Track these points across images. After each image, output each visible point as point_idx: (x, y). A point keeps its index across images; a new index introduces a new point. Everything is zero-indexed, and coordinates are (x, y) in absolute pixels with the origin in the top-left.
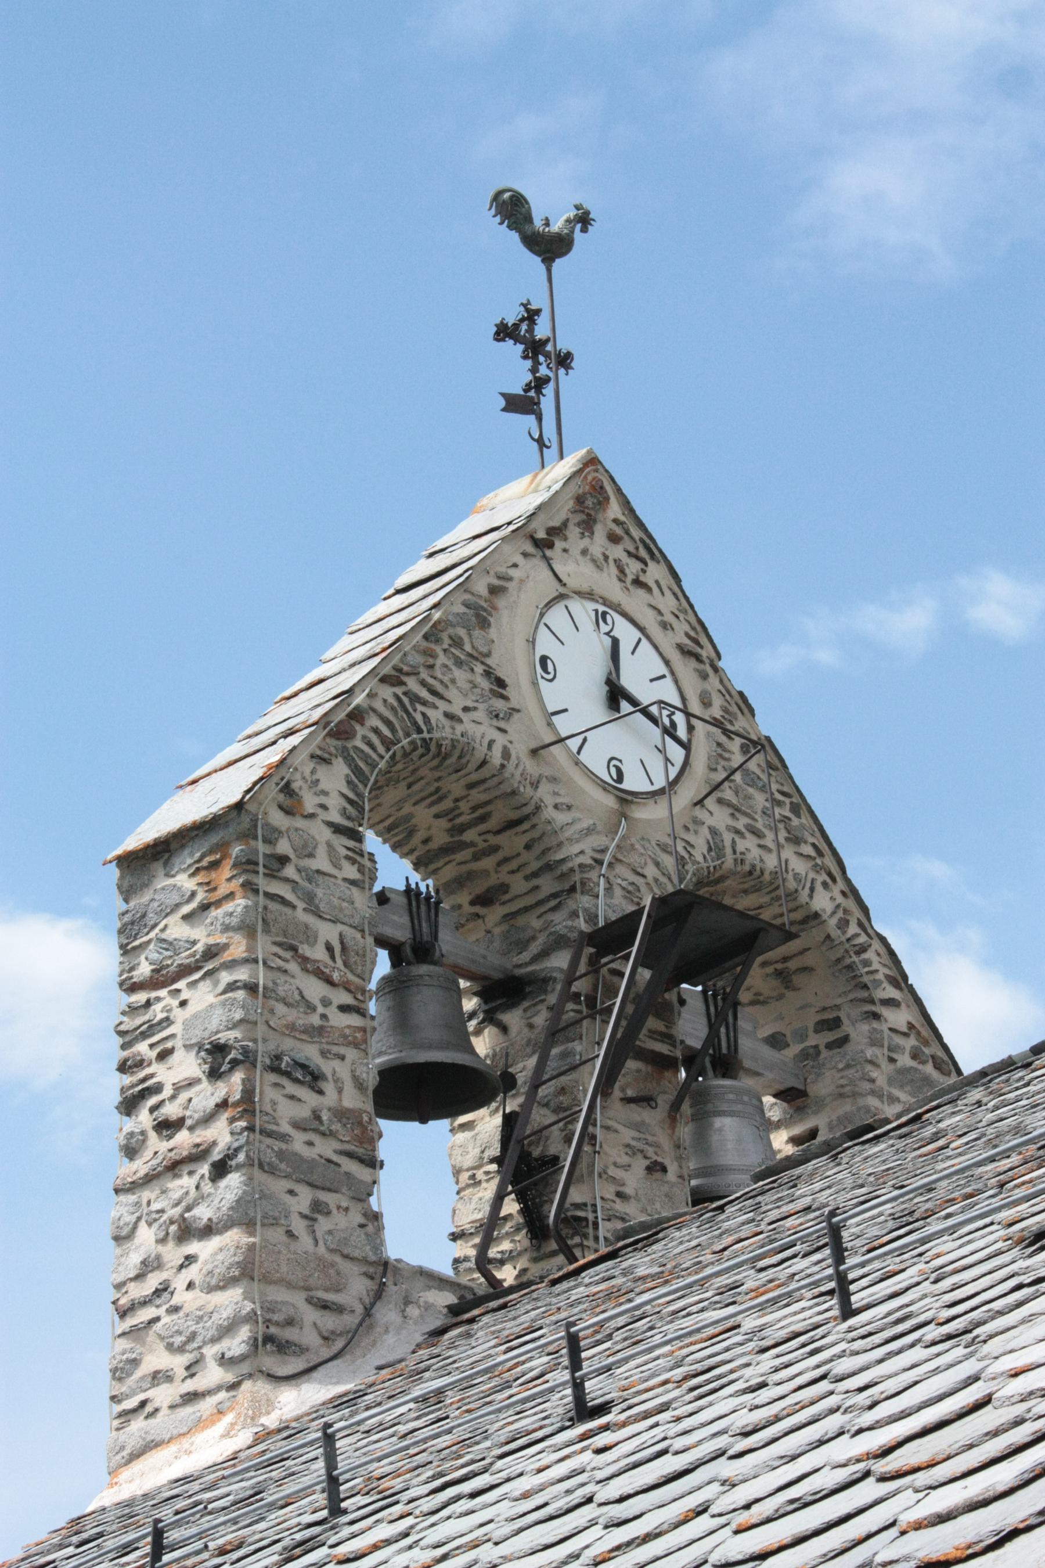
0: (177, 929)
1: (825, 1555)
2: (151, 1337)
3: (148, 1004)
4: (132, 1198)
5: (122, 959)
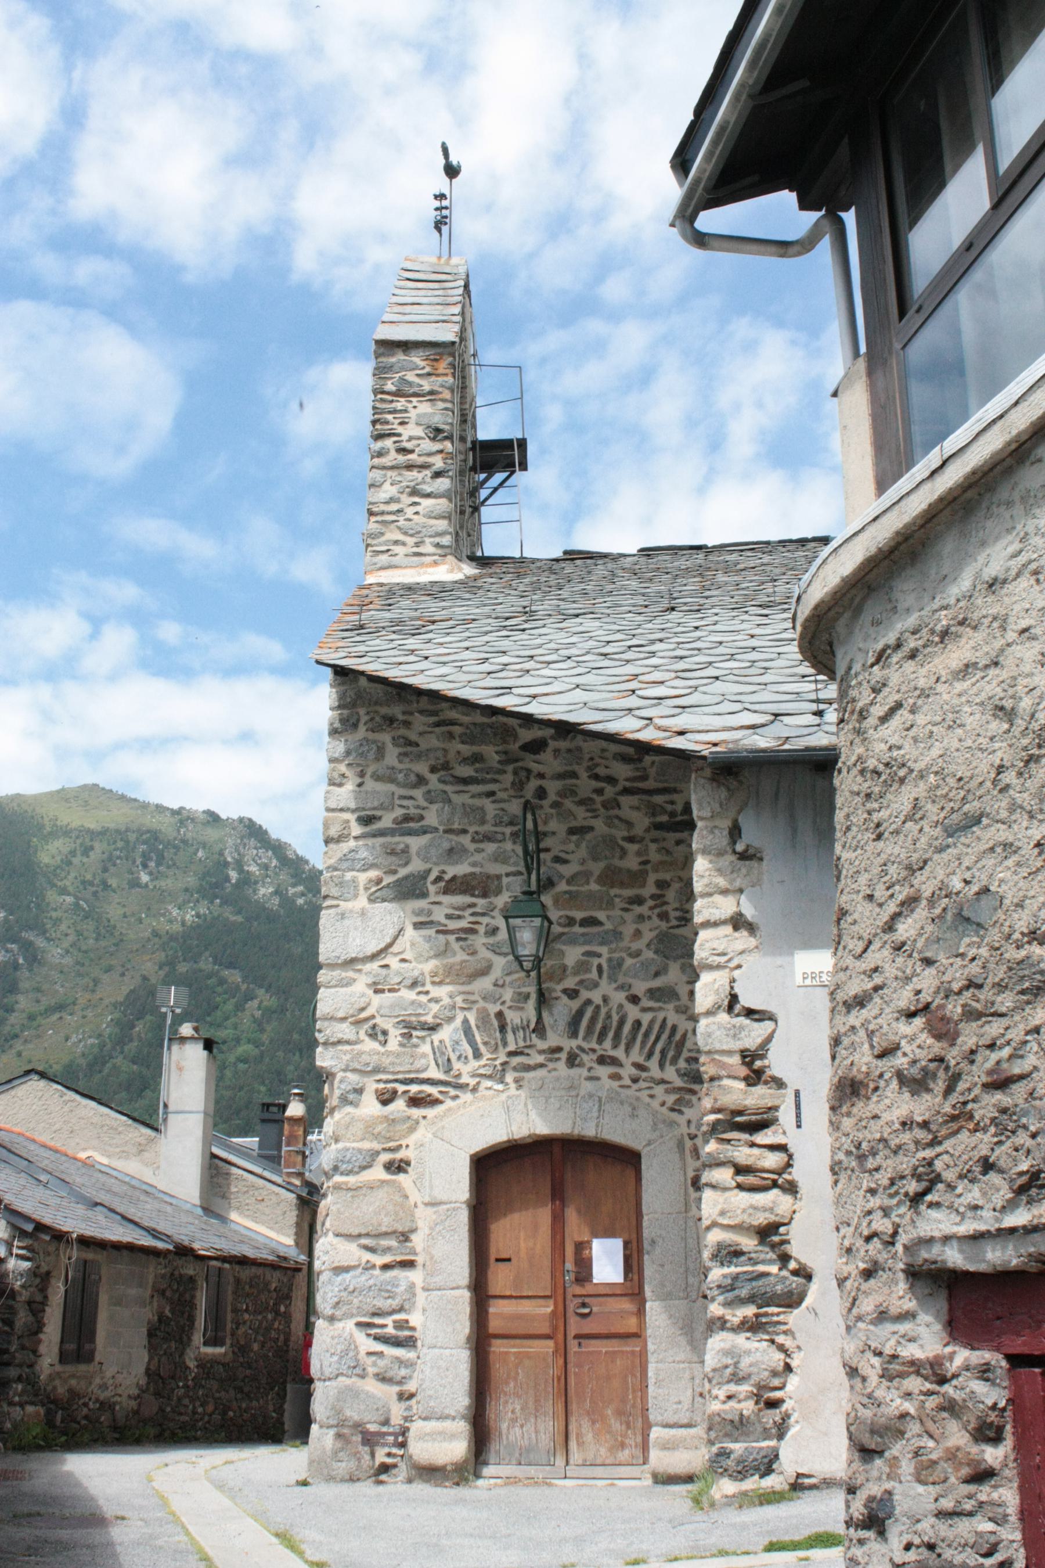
0: (411, 377)
2: (393, 526)
3: (392, 401)
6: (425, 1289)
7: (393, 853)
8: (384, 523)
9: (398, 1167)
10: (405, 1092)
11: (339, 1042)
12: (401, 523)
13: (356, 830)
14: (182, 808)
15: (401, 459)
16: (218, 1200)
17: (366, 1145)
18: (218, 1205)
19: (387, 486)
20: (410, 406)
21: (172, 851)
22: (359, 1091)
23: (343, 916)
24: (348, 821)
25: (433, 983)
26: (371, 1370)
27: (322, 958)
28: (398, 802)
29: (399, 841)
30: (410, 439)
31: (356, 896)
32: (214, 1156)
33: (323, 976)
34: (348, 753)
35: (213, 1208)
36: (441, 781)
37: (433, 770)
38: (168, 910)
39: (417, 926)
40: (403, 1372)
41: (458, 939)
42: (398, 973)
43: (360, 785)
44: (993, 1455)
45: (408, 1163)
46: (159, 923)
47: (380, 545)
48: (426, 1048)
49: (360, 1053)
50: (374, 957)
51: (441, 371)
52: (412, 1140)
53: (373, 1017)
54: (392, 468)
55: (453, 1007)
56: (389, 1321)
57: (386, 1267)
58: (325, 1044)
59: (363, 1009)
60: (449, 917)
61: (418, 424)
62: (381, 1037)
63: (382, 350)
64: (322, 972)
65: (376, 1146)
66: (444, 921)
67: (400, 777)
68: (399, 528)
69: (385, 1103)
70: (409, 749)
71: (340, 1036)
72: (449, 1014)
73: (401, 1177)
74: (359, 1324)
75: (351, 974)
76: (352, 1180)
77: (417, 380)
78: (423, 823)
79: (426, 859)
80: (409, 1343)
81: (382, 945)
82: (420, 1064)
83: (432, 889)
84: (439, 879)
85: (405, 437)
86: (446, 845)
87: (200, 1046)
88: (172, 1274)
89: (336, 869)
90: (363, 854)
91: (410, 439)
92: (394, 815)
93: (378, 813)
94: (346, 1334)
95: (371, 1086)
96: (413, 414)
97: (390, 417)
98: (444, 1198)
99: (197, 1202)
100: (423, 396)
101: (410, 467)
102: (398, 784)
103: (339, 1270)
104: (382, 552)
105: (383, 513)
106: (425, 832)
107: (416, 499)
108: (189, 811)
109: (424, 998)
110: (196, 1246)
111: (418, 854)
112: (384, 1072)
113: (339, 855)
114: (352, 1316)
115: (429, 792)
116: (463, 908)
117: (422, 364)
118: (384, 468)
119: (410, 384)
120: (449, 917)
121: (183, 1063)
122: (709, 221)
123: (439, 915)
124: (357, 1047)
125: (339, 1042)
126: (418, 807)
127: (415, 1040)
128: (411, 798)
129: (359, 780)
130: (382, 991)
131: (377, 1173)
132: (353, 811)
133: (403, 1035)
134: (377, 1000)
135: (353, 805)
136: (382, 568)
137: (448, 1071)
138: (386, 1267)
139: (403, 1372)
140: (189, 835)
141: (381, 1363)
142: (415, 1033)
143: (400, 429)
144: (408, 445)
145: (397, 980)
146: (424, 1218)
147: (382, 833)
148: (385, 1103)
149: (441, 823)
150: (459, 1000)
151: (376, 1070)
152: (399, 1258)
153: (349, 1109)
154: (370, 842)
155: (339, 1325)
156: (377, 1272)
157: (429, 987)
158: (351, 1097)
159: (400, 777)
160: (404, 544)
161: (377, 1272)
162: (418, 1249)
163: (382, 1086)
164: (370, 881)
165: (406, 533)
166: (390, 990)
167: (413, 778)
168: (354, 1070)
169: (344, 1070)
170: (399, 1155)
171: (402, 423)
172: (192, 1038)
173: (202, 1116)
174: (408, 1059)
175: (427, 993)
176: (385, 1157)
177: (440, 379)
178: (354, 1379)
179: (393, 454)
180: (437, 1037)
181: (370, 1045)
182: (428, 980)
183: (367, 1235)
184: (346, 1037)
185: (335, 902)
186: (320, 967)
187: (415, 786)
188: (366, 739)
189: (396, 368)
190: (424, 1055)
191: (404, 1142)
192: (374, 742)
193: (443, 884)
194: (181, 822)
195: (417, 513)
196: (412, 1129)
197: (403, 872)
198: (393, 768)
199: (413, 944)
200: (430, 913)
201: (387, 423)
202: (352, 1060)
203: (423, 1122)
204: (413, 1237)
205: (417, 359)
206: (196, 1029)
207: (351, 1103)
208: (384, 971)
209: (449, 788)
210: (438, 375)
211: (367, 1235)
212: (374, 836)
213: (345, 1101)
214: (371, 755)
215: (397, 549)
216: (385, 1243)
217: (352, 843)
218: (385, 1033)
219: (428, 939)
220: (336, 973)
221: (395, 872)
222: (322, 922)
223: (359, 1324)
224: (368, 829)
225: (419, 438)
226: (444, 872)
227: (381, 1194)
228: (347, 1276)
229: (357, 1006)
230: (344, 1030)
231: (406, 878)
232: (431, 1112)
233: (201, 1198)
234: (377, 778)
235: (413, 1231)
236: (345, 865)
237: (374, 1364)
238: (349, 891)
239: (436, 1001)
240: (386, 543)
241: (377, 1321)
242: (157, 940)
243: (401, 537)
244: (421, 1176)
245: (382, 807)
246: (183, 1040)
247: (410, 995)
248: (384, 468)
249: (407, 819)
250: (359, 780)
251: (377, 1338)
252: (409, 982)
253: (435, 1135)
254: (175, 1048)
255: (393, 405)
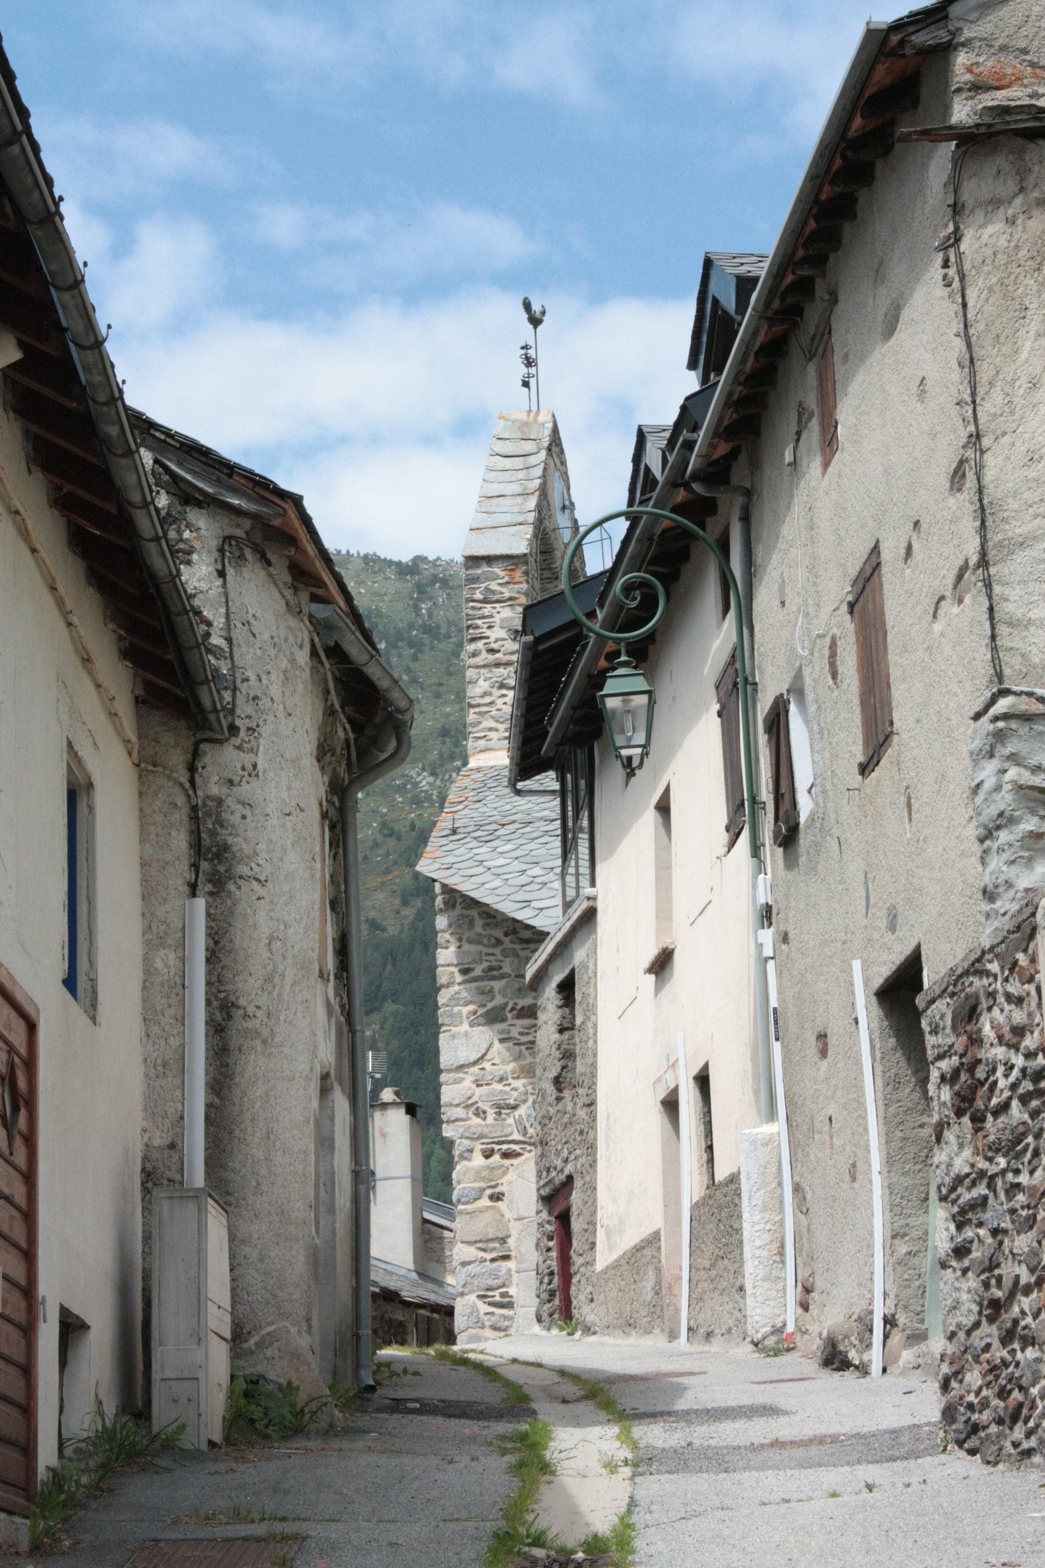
0: (494, 586)
1: (736, 808)
2: (487, 716)
3: (481, 608)
4: (477, 670)
5: (144, 1124)
6: (517, 1272)
7: (483, 993)
8: (480, 714)
9: (497, 1197)
10: (500, 1150)
11: (456, 1120)
12: (494, 713)
13: (459, 978)
14: (419, 559)
15: (491, 658)
16: (433, 1265)
17: (477, 1185)
18: (433, 1269)
19: (481, 682)
20: (494, 611)
21: (408, 652)
22: (471, 1151)
23: (453, 1037)
24: (453, 973)
25: (513, 1078)
26: (487, 1324)
27: (442, 1066)
28: (485, 958)
29: (486, 984)
30: (497, 640)
31: (461, 1023)
32: (426, 1221)
33: (443, 1077)
34: (450, 925)
35: (430, 1273)
36: (512, 942)
37: (506, 934)
38: (409, 779)
39: (502, 1041)
40: (507, 1323)
41: (527, 1048)
42: (491, 1073)
43: (459, 947)
44: (551, 1244)
45: (503, 1195)
46: (392, 806)
47: (478, 732)
48: (511, 1121)
49: (470, 1127)
50: (475, 1063)
51: (517, 579)
52: (505, 1180)
53: (477, 1102)
54: (484, 666)
55: (526, 1093)
56: (496, 1293)
57: (493, 1260)
58: (448, 1122)
59: (470, 1098)
60: (521, 1034)
61: (502, 627)
62: (482, 1116)
63: (470, 564)
64: (443, 1074)
65: (483, 1185)
66: (518, 1037)
67: (485, 940)
68: (492, 717)
69: (487, 1157)
70: (489, 920)
71: (456, 1116)
72: (524, 1098)
73: (499, 1204)
74: (479, 1297)
75: (461, 1075)
76: (469, 1207)
77: (498, 588)
78: (502, 971)
79: (504, 996)
80: (509, 1305)
81: (479, 1055)
82: (507, 1131)
83: (509, 1015)
84: (513, 1009)
85: (492, 640)
86: (517, 986)
87: (402, 1111)
88: (382, 1317)
89: (447, 1006)
90: (464, 994)
91: (497, 640)
92: (482, 967)
93: (472, 966)
94: (471, 1303)
95: (478, 1147)
96: (497, 618)
97: (479, 622)
98: (526, 1215)
99: (412, 1267)
100: (504, 602)
101: (497, 665)
102: (484, 945)
103: (464, 1264)
104: (480, 738)
105: (479, 705)
106: (502, 978)
107: (504, 692)
108: (434, 563)
109: (507, 1088)
110: (403, 1293)
111: (499, 992)
112: (486, 1137)
113: (449, 996)
114: (475, 1292)
115: (504, 950)
116: (529, 1028)
117: (502, 574)
118: (477, 667)
119: (493, 592)
120: (521, 1034)
121: (386, 1130)
122: (520, 785)
123: (515, 1033)
124: (468, 1122)
125: (456, 1120)
126: (497, 961)
127: (503, 1116)
128: (493, 954)
129: (458, 944)
130: (481, 1085)
131: (484, 1202)
132: (456, 966)
133: (496, 1113)
134: (478, 1091)
135: (455, 962)
136: (481, 751)
137: (525, 1135)
138: (493, 1260)
139: (507, 1323)
140: (440, 615)
141: (493, 1319)
142: (503, 1111)
143: (488, 633)
144: (495, 646)
145: (490, 1077)
146: (514, 1228)
147: (475, 980)
148: (487, 1157)
149: (513, 971)
150: (529, 1088)
151: (481, 1137)
152: (501, 1254)
153: (465, 1163)
154: (468, 986)
155: (467, 1298)
156: (488, 1263)
157: (510, 1081)
158: (466, 1155)
159: (485, 940)
160: (497, 730)
161: (488, 1263)
162: (512, 1248)
163: (485, 1146)
164: (470, 1013)
165: (497, 721)
166: (487, 1084)
167: (493, 941)
168: (467, 1138)
169: (461, 1138)
170: (497, 1190)
171: (489, 627)
172: (394, 1104)
173: (409, 1180)
174: (499, 1128)
175: (509, 1085)
176: (489, 1192)
177: (516, 586)
178: (478, 1330)
179: (484, 653)
180: (517, 1113)
181: (476, 1121)
182: (510, 1077)
183: (480, 1241)
184: (460, 1117)
185: (448, 1028)
186: (441, 1071)
187: (494, 946)
188: (462, 915)
189: (482, 579)
190: (510, 1125)
191: (500, 1182)
192: (467, 916)
193: (515, 1012)
194: (420, 588)
195: (505, 703)
196: (505, 1173)
197: (490, 1006)
198: (480, 935)
199: (499, 1053)
200: (509, 1032)
201: (477, 627)
202: (465, 1131)
203: (511, 1168)
204: (509, 1240)
205: (497, 570)
206: (397, 1094)
207: (466, 1159)
208: (482, 1072)
209: (517, 947)
210: (515, 583)
211: (480, 1241)
212: (470, 982)
213: (462, 1157)
214: (465, 927)
215: (493, 735)
216: (491, 1245)
217: (457, 988)
218: (484, 1112)
219: (508, 1049)
220: (452, 1075)
221: (484, 1006)
222: (441, 1042)
223: (479, 1297)
224: (466, 977)
225: (504, 639)
226: (516, 1004)
227: (487, 1216)
228: (470, 1267)
229: (466, 1096)
230: (460, 1112)
231: (492, 1009)
232: (515, 1162)
233: (415, 1262)
234: (470, 941)
235: (509, 1236)
236: (453, 1003)
237: (489, 1320)
238: (457, 1019)
239: (515, 1089)
240: (483, 730)
241: (490, 1293)
242: (392, 842)
243: (494, 725)
244: (511, 1202)
245: (474, 962)
246: (385, 1106)
247: (499, 1087)
248: (477, 667)
249: (491, 969)
250: (458, 944)
251: (490, 1304)
252: (498, 1078)
253: (518, 1175)
254: (377, 1115)
255: (481, 612)
